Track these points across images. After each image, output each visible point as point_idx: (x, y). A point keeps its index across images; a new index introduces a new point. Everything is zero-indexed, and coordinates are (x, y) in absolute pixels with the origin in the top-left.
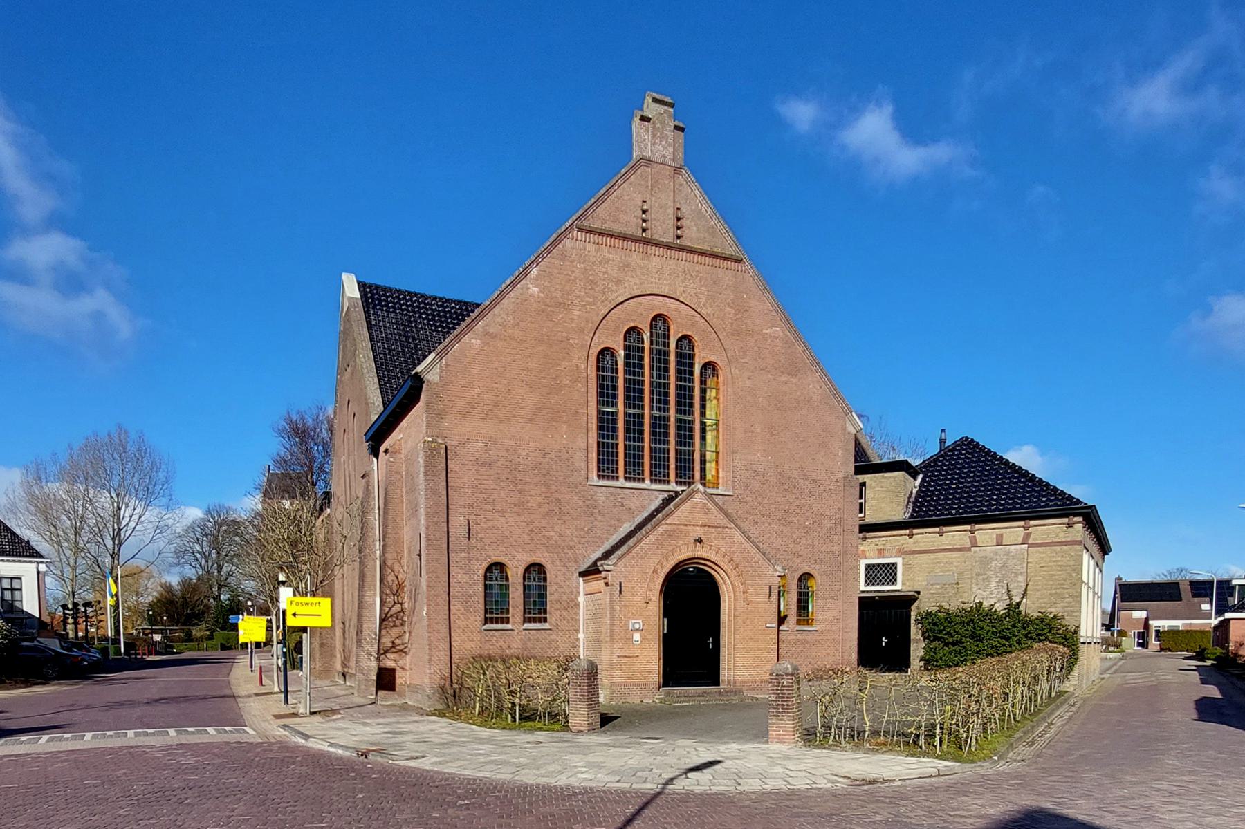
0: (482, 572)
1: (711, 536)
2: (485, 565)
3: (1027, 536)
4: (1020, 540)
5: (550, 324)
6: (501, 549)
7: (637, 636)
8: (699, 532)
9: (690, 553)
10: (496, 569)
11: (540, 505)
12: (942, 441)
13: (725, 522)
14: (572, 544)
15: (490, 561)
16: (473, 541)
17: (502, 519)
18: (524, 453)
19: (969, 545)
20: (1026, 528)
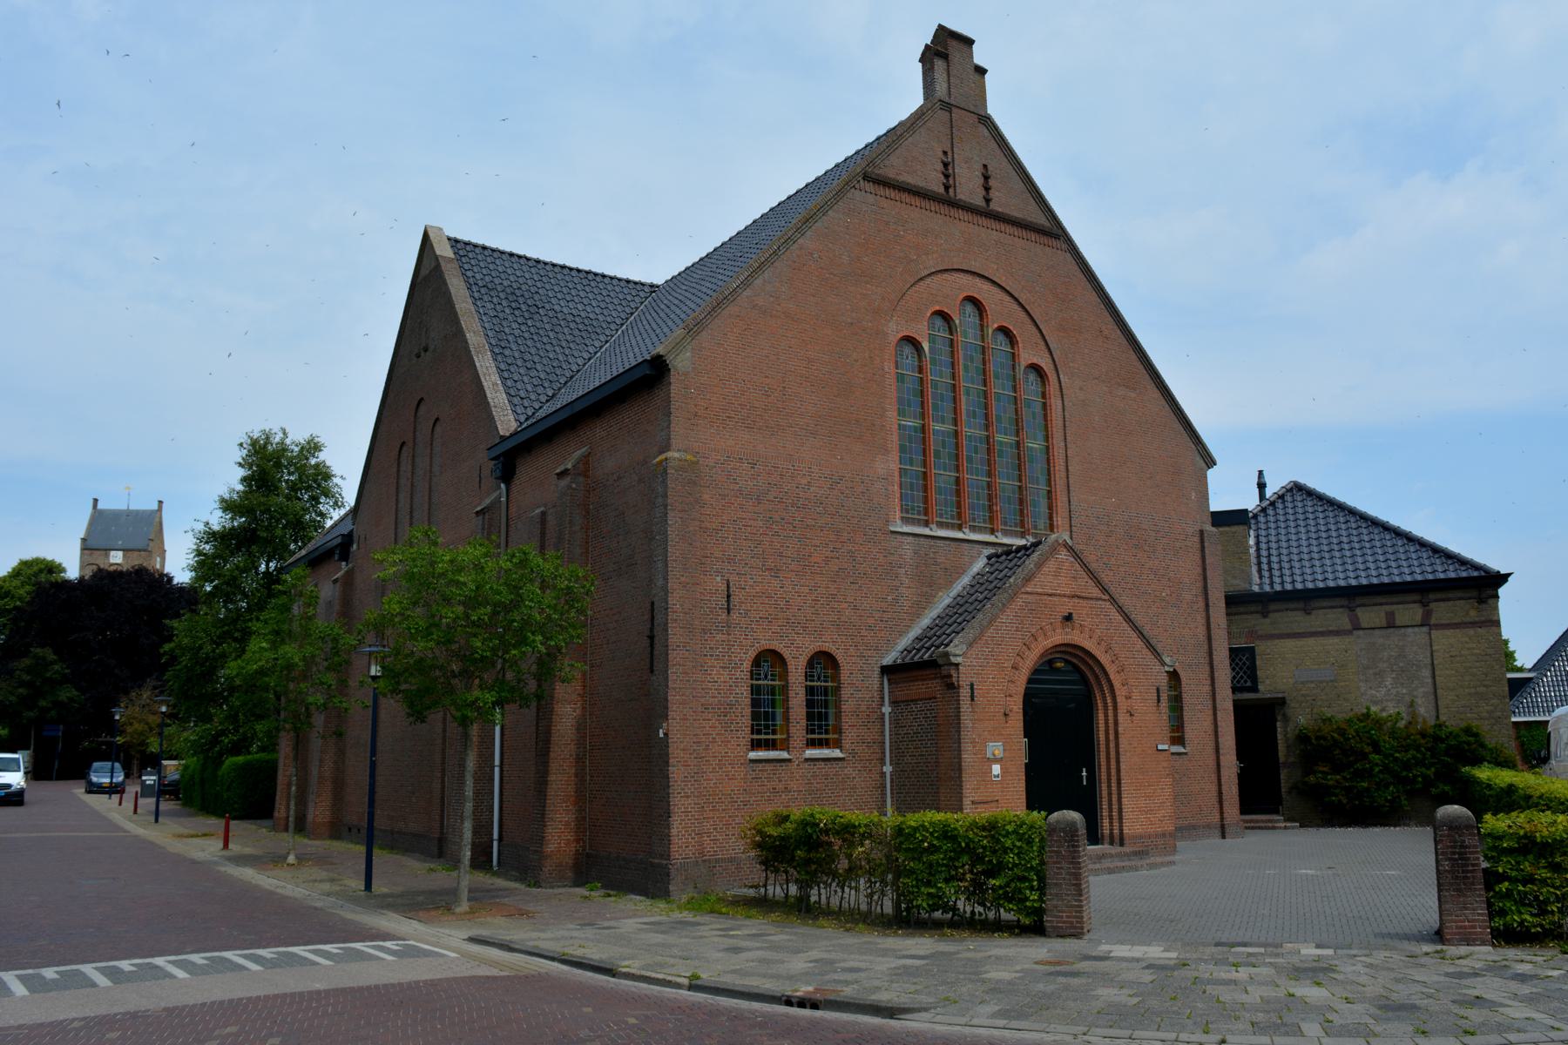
0: (747, 665)
1: (1082, 611)
2: (752, 654)
3: (1427, 615)
4: (1418, 618)
5: (403, 687)
6: (775, 628)
7: (996, 769)
8: (1067, 606)
9: (1058, 637)
10: (769, 660)
11: (827, 560)
12: (1262, 486)
13: (1096, 592)
14: (871, 621)
15: (758, 647)
16: (735, 615)
17: (776, 583)
18: (804, 481)
19: (1349, 627)
20: (1425, 605)
